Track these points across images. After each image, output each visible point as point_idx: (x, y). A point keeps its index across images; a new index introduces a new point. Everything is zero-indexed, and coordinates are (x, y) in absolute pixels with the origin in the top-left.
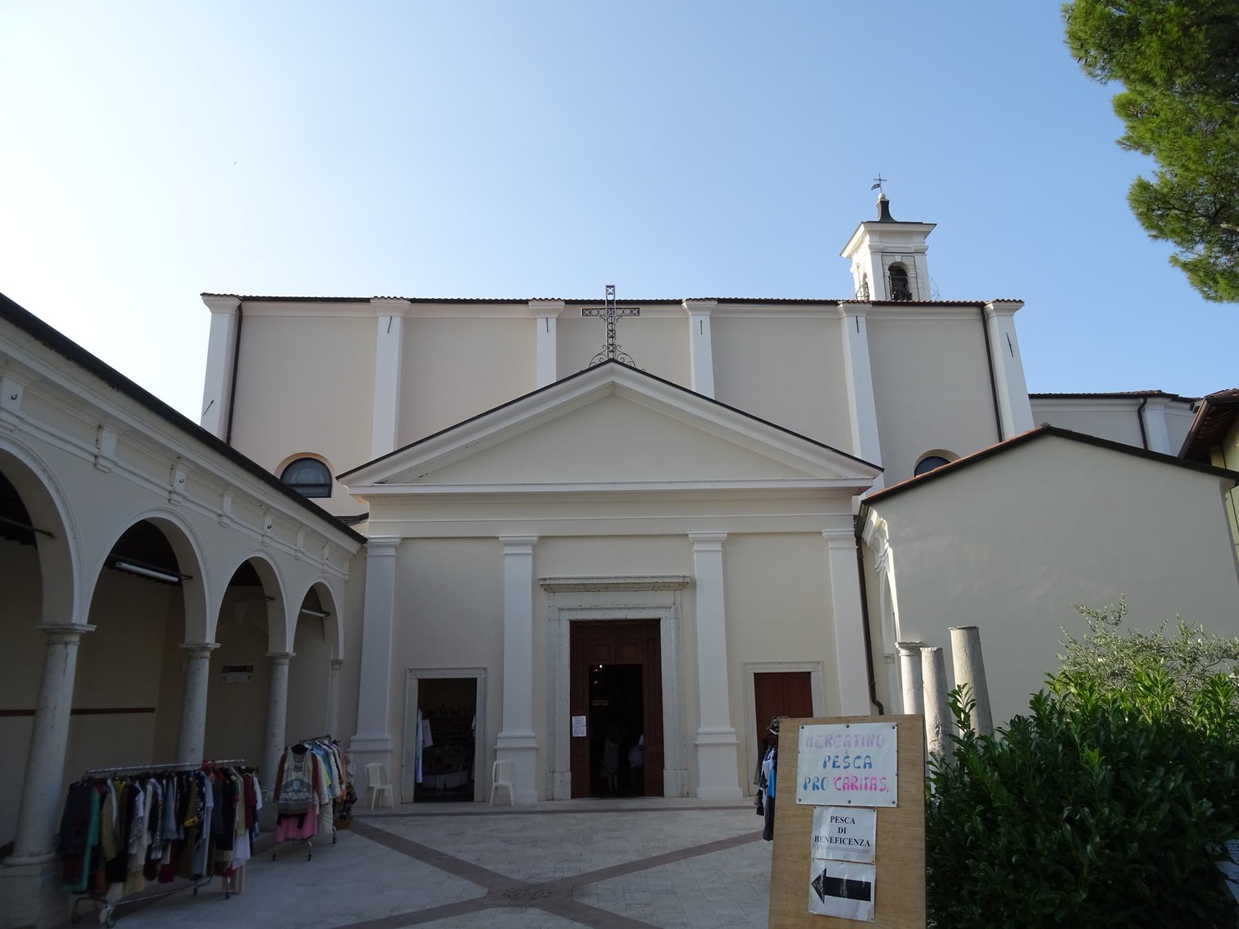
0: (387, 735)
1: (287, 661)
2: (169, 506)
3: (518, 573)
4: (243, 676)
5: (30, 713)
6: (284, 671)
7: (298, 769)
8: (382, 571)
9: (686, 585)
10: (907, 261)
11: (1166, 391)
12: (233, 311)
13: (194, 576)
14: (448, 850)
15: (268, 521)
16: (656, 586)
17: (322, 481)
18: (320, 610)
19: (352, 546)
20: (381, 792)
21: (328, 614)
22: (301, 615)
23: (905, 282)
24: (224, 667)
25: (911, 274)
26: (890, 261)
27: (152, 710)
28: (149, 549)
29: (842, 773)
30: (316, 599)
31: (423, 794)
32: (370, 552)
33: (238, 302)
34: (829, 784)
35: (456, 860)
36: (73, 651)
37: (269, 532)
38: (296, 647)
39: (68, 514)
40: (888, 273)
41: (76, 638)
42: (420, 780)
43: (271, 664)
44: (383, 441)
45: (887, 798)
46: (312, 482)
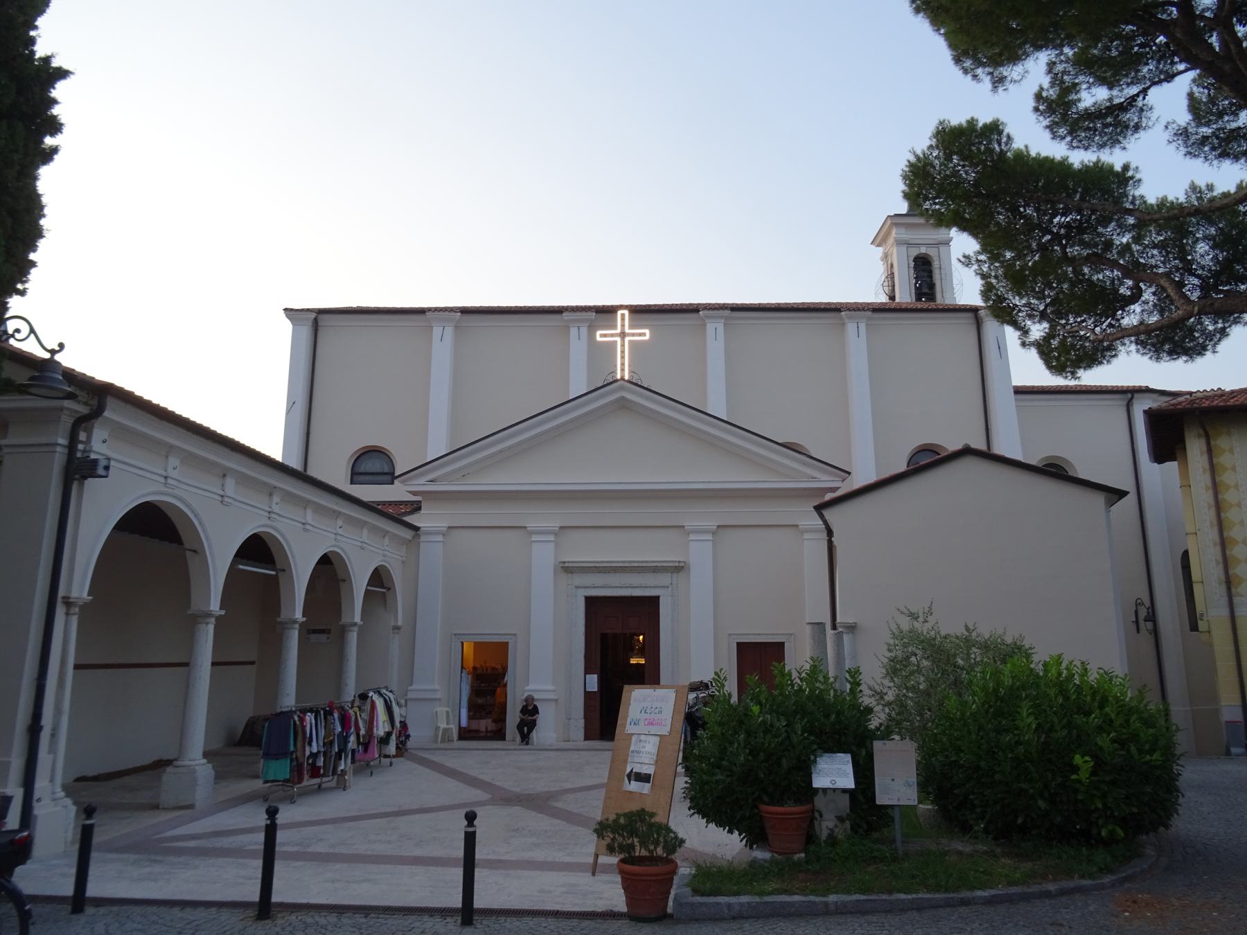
0: (436, 687)
1: (356, 629)
2: (269, 522)
3: (544, 556)
4: (323, 637)
5: (186, 665)
6: (353, 637)
8: (432, 552)
9: (679, 569)
10: (932, 252)
11: (1151, 386)
12: (310, 323)
13: (286, 570)
14: (473, 772)
15: (340, 523)
16: (656, 569)
17: (386, 470)
18: (382, 587)
19: (407, 534)
20: (445, 730)
21: (389, 589)
22: (367, 591)
23: (930, 274)
24: (308, 631)
25: (936, 264)
26: (915, 252)
27: (252, 663)
29: (647, 716)
30: (379, 578)
31: (466, 734)
32: (423, 538)
33: (314, 315)
34: (641, 723)
35: (476, 779)
36: (211, 628)
37: (340, 531)
39: (196, 516)
40: (912, 264)
41: (213, 620)
42: (464, 723)
43: (343, 631)
45: (665, 730)
46: (379, 470)
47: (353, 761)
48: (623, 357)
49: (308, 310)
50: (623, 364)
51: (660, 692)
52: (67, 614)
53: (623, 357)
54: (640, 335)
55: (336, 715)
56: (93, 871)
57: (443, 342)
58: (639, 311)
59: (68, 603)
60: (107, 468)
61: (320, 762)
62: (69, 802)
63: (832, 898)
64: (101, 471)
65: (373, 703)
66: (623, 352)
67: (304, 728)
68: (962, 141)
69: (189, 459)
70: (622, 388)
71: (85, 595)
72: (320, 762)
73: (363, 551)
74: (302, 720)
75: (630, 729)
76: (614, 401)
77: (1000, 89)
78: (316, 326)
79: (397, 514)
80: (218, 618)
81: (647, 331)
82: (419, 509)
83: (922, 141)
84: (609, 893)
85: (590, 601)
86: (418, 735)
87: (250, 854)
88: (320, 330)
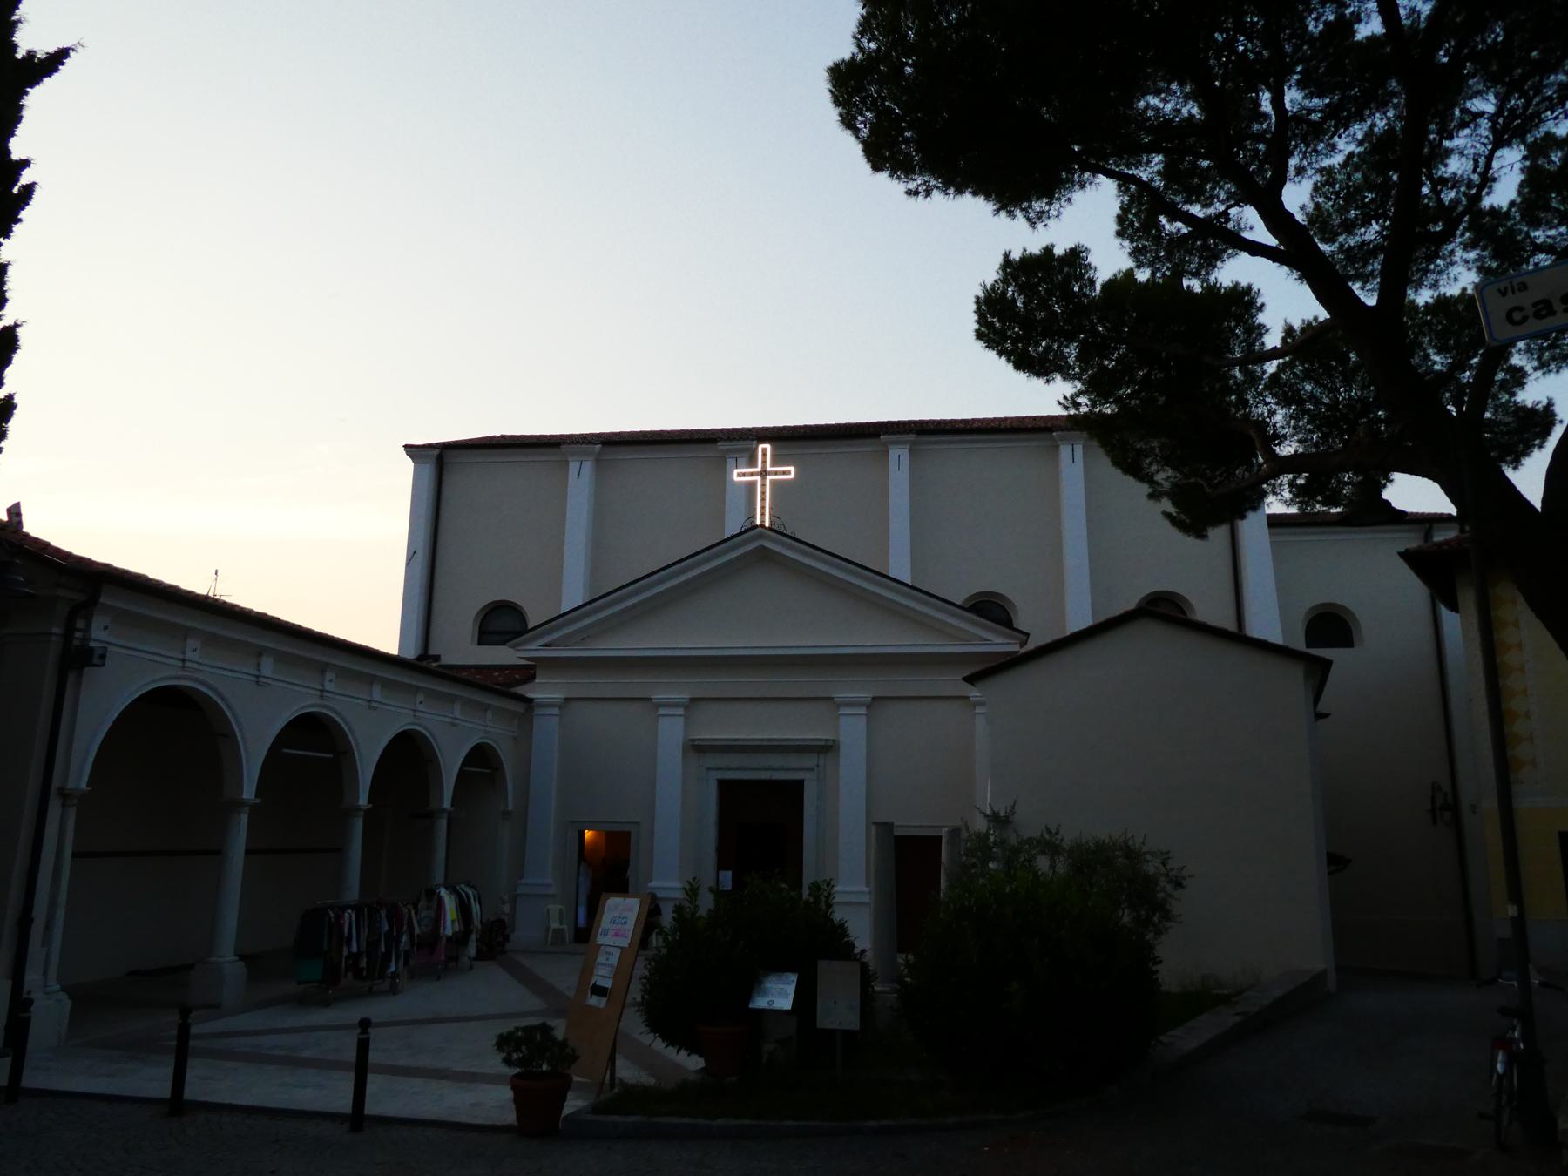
0: (551, 881)
2: (319, 702)
3: (671, 732)
6: (443, 824)
7: (428, 908)
8: (547, 727)
9: (827, 749)
19: (518, 708)
28: (313, 733)
32: (537, 711)
33: (436, 452)
36: (244, 818)
37: (420, 707)
38: (455, 800)
44: (573, 595)
47: (406, 963)
48: (763, 499)
49: (430, 446)
50: (763, 508)
51: (629, 901)
52: (63, 805)
53: (763, 499)
54: (784, 473)
55: (383, 913)
56: (190, 1076)
57: (580, 478)
58: (788, 439)
59: (64, 795)
60: (103, 657)
61: (363, 964)
62: (64, 996)
63: (720, 1121)
64: (96, 661)
65: (440, 901)
66: (763, 493)
67: (341, 927)
68: (1029, 273)
69: (211, 640)
70: (760, 536)
71: (83, 786)
72: (363, 964)
73: (453, 733)
74: (339, 917)
75: (601, 940)
76: (759, 554)
77: (1040, 226)
78: (440, 463)
79: (502, 685)
80: (253, 808)
81: (792, 469)
82: (533, 677)
83: (990, 274)
84: (494, 1102)
85: (724, 785)
86: (524, 933)
87: (336, 1065)
88: (449, 471)
